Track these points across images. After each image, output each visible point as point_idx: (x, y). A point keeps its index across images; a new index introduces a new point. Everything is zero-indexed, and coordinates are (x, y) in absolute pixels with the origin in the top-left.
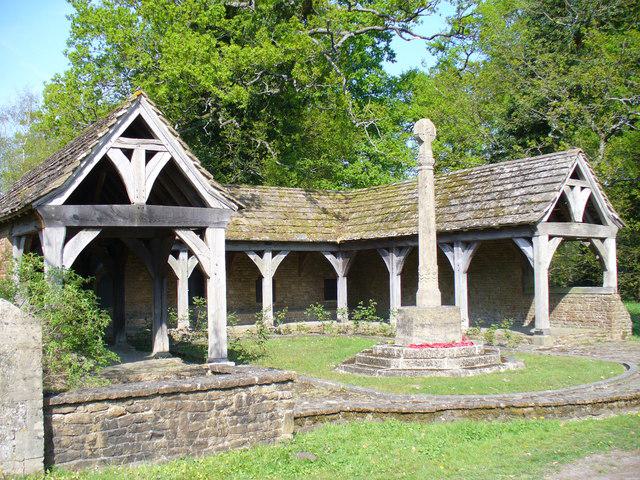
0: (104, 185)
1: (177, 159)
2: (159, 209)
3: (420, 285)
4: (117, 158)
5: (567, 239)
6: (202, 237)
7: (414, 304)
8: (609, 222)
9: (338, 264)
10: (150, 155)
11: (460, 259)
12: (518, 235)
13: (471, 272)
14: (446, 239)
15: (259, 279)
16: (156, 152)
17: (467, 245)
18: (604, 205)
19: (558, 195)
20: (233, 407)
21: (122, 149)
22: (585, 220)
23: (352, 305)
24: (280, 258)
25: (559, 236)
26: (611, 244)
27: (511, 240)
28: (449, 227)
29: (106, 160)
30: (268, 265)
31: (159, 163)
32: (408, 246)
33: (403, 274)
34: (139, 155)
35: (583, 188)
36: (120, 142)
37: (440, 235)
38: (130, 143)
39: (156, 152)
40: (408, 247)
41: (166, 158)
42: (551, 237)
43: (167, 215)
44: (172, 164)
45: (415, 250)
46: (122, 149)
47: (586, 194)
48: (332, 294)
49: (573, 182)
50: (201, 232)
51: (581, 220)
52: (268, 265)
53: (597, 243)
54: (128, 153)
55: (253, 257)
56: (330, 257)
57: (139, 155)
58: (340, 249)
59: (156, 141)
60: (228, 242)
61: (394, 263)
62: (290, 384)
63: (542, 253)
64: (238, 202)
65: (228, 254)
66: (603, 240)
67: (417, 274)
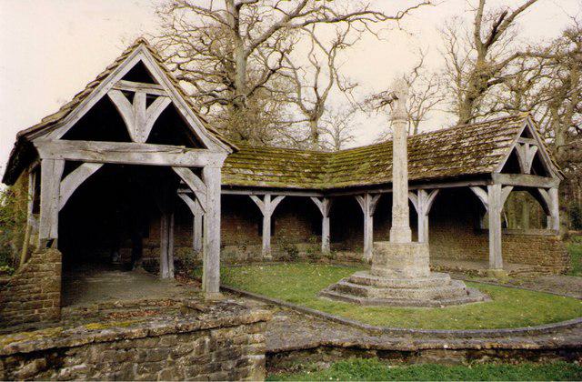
1: (177, 104)
3: (393, 224)
4: (118, 99)
5: (517, 188)
7: (387, 239)
8: (553, 175)
9: (323, 206)
10: (150, 100)
11: (424, 203)
12: (473, 184)
13: (432, 215)
14: (414, 185)
15: (261, 216)
16: (157, 96)
17: (429, 192)
19: (508, 152)
20: (193, 354)
22: (532, 173)
24: (278, 200)
25: (511, 185)
26: (554, 192)
28: (414, 178)
31: (160, 106)
32: (384, 197)
33: (375, 216)
34: (141, 97)
35: (531, 146)
37: (411, 183)
38: (131, 86)
39: (157, 96)
40: (436, 189)
41: (167, 102)
42: (503, 186)
47: (535, 149)
48: (319, 232)
49: (523, 140)
51: (529, 172)
53: (542, 192)
54: (130, 96)
55: (255, 199)
56: (316, 201)
57: (141, 97)
58: (324, 194)
59: (157, 86)
60: (223, 187)
61: (367, 205)
62: (262, 324)
63: (494, 198)
64: (233, 145)
65: (223, 197)
66: (547, 189)
67: (391, 214)
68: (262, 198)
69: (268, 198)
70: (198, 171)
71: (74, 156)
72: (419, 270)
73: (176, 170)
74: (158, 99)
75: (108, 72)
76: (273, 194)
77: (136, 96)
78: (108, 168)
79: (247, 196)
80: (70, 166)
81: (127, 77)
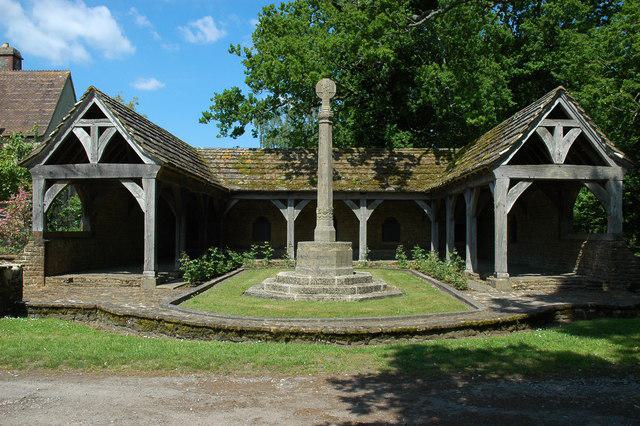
0: (72, 151)
2: (105, 166)
4: (80, 133)
6: (140, 185)
17: (296, 205)
18: (595, 139)
21: (83, 128)
23: (370, 257)
27: (269, 201)
29: (72, 136)
30: (363, 214)
34: (559, 130)
36: (82, 123)
38: (551, 123)
43: (113, 170)
44: (582, 136)
45: (314, 203)
46: (83, 128)
50: (138, 181)
52: (363, 214)
54: (87, 129)
57: (559, 130)
76: (296, 197)
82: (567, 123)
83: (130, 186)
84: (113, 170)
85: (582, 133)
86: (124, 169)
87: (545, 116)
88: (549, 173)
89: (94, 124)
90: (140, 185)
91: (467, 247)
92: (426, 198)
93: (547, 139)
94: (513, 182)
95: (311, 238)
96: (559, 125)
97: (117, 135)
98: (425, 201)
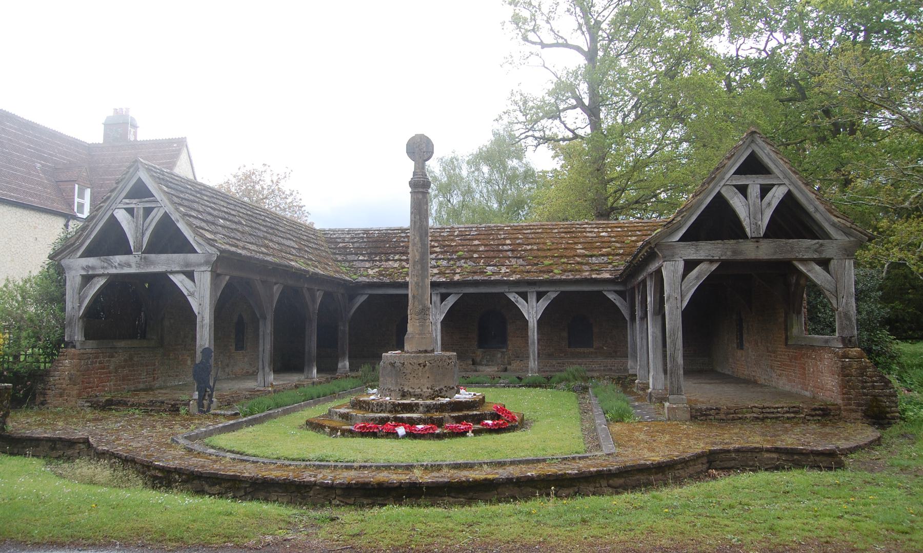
10: (765, 190)
16: (773, 185)
24: (451, 301)
31: (776, 195)
34: (754, 191)
38: (742, 180)
54: (130, 211)
55: (513, 297)
57: (754, 191)
68: (524, 296)
69: (532, 298)
70: (87, 279)
71: (693, 257)
72: (445, 471)
73: (171, 277)
74: (774, 189)
75: (124, 176)
76: (444, 291)
77: (749, 190)
78: (725, 264)
79: (600, 292)
80: (690, 265)
81: (739, 172)
82: (766, 181)
83: (179, 280)
84: (161, 263)
85: (789, 191)
86: (803, 247)
87: (733, 171)
88: (752, 251)
89: (138, 205)
90: (193, 280)
91: (274, 306)
92: (618, 288)
93: (737, 203)
94: (690, 265)
95: (400, 346)
96: (754, 184)
97: (166, 216)
98: (616, 292)
